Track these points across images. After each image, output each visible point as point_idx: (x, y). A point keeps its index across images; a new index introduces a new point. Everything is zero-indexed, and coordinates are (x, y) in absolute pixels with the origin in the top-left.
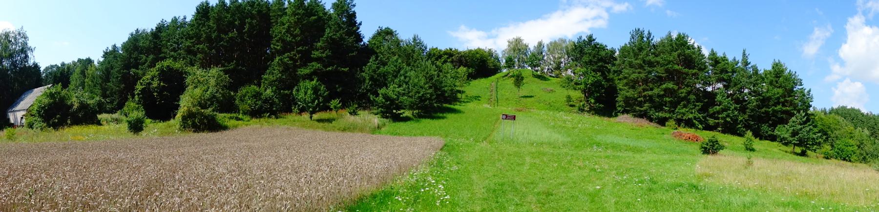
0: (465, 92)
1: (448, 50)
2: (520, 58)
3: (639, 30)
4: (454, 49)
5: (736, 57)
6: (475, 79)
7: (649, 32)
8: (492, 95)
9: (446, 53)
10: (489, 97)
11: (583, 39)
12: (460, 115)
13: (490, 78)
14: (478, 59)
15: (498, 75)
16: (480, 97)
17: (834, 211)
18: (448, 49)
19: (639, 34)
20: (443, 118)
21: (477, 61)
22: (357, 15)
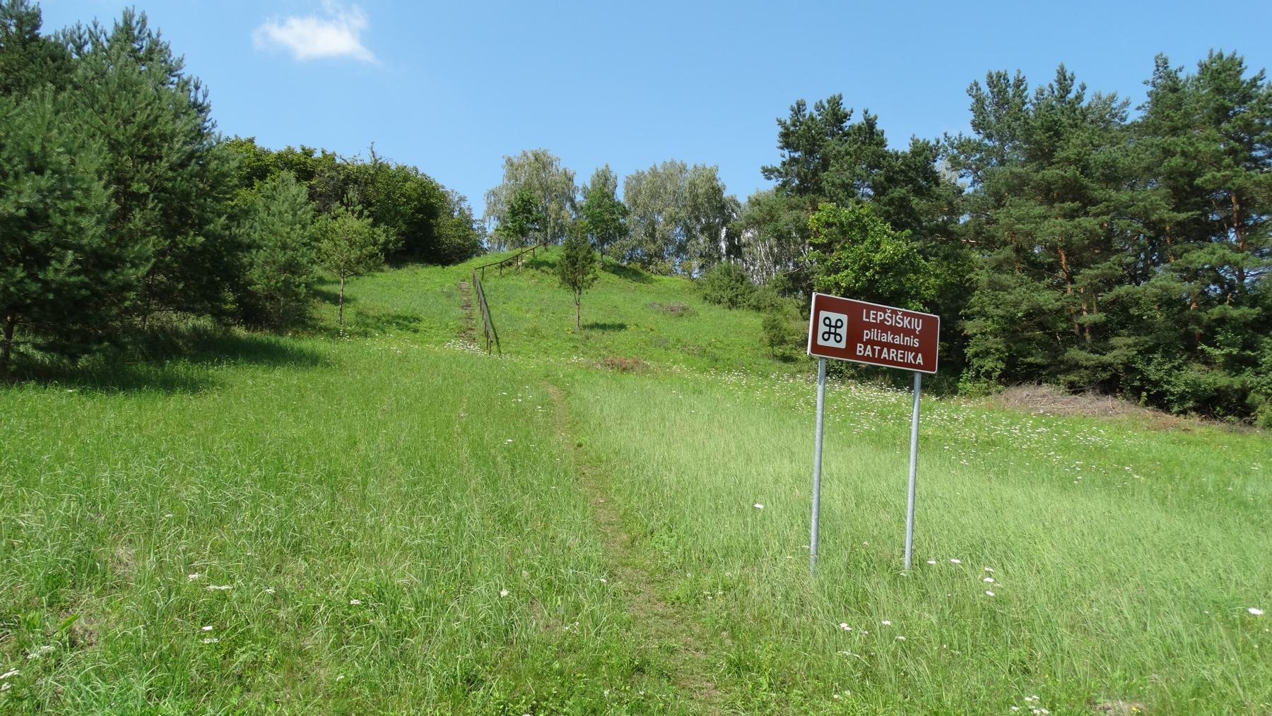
0: (355, 299)
1: (293, 153)
2: (640, 192)
3: (1221, 56)
4: (318, 155)
5: (1066, 67)
6: (399, 268)
7: (1073, 74)
8: (469, 318)
9: (286, 161)
10: (461, 323)
11: (807, 113)
12: (314, 374)
13: (452, 268)
14: (409, 199)
15: (476, 262)
16: (418, 319)
17: (1271, 190)
18: (299, 151)
19: (289, 148)
20: (193, 386)
21: (407, 203)
22: (43, 16)
